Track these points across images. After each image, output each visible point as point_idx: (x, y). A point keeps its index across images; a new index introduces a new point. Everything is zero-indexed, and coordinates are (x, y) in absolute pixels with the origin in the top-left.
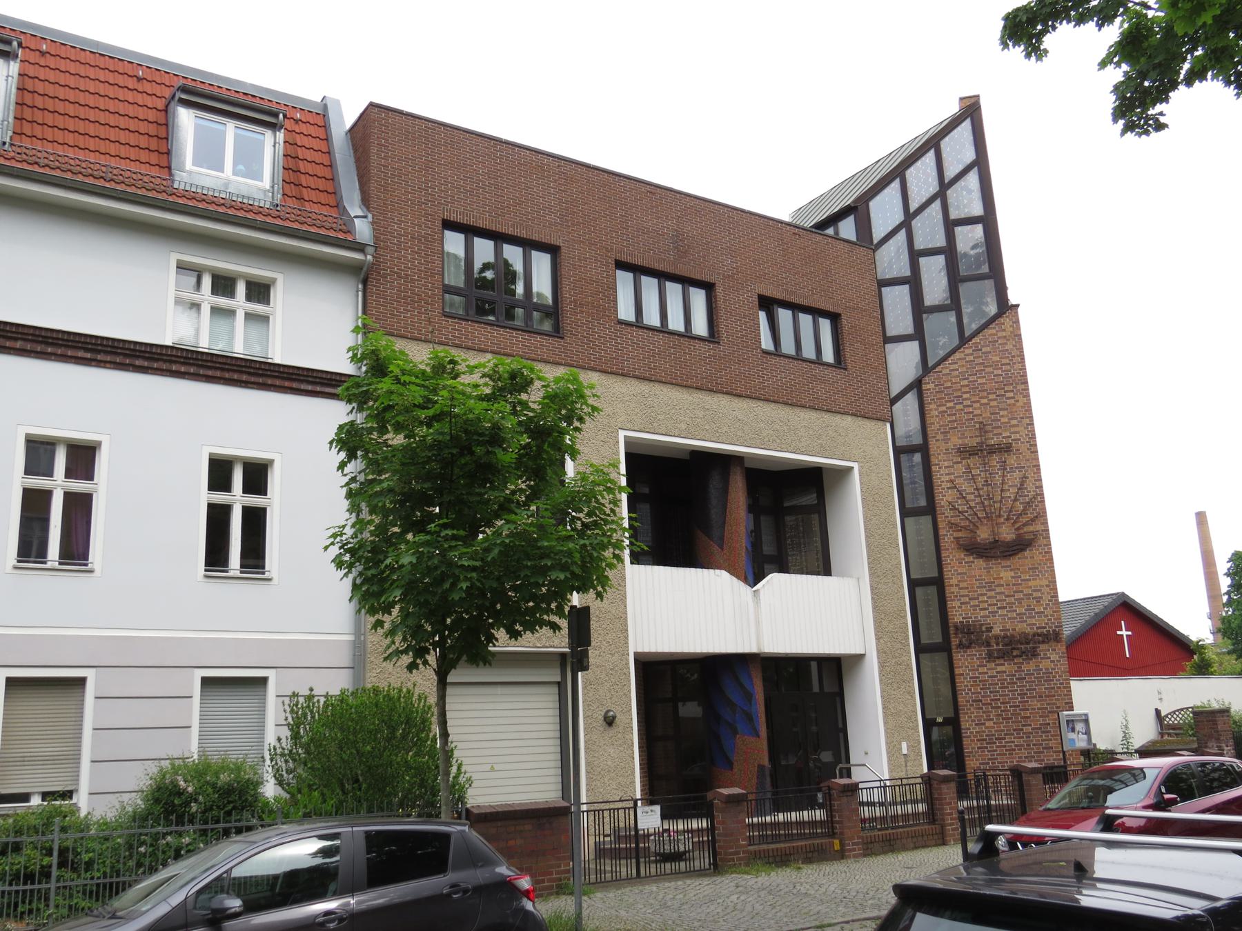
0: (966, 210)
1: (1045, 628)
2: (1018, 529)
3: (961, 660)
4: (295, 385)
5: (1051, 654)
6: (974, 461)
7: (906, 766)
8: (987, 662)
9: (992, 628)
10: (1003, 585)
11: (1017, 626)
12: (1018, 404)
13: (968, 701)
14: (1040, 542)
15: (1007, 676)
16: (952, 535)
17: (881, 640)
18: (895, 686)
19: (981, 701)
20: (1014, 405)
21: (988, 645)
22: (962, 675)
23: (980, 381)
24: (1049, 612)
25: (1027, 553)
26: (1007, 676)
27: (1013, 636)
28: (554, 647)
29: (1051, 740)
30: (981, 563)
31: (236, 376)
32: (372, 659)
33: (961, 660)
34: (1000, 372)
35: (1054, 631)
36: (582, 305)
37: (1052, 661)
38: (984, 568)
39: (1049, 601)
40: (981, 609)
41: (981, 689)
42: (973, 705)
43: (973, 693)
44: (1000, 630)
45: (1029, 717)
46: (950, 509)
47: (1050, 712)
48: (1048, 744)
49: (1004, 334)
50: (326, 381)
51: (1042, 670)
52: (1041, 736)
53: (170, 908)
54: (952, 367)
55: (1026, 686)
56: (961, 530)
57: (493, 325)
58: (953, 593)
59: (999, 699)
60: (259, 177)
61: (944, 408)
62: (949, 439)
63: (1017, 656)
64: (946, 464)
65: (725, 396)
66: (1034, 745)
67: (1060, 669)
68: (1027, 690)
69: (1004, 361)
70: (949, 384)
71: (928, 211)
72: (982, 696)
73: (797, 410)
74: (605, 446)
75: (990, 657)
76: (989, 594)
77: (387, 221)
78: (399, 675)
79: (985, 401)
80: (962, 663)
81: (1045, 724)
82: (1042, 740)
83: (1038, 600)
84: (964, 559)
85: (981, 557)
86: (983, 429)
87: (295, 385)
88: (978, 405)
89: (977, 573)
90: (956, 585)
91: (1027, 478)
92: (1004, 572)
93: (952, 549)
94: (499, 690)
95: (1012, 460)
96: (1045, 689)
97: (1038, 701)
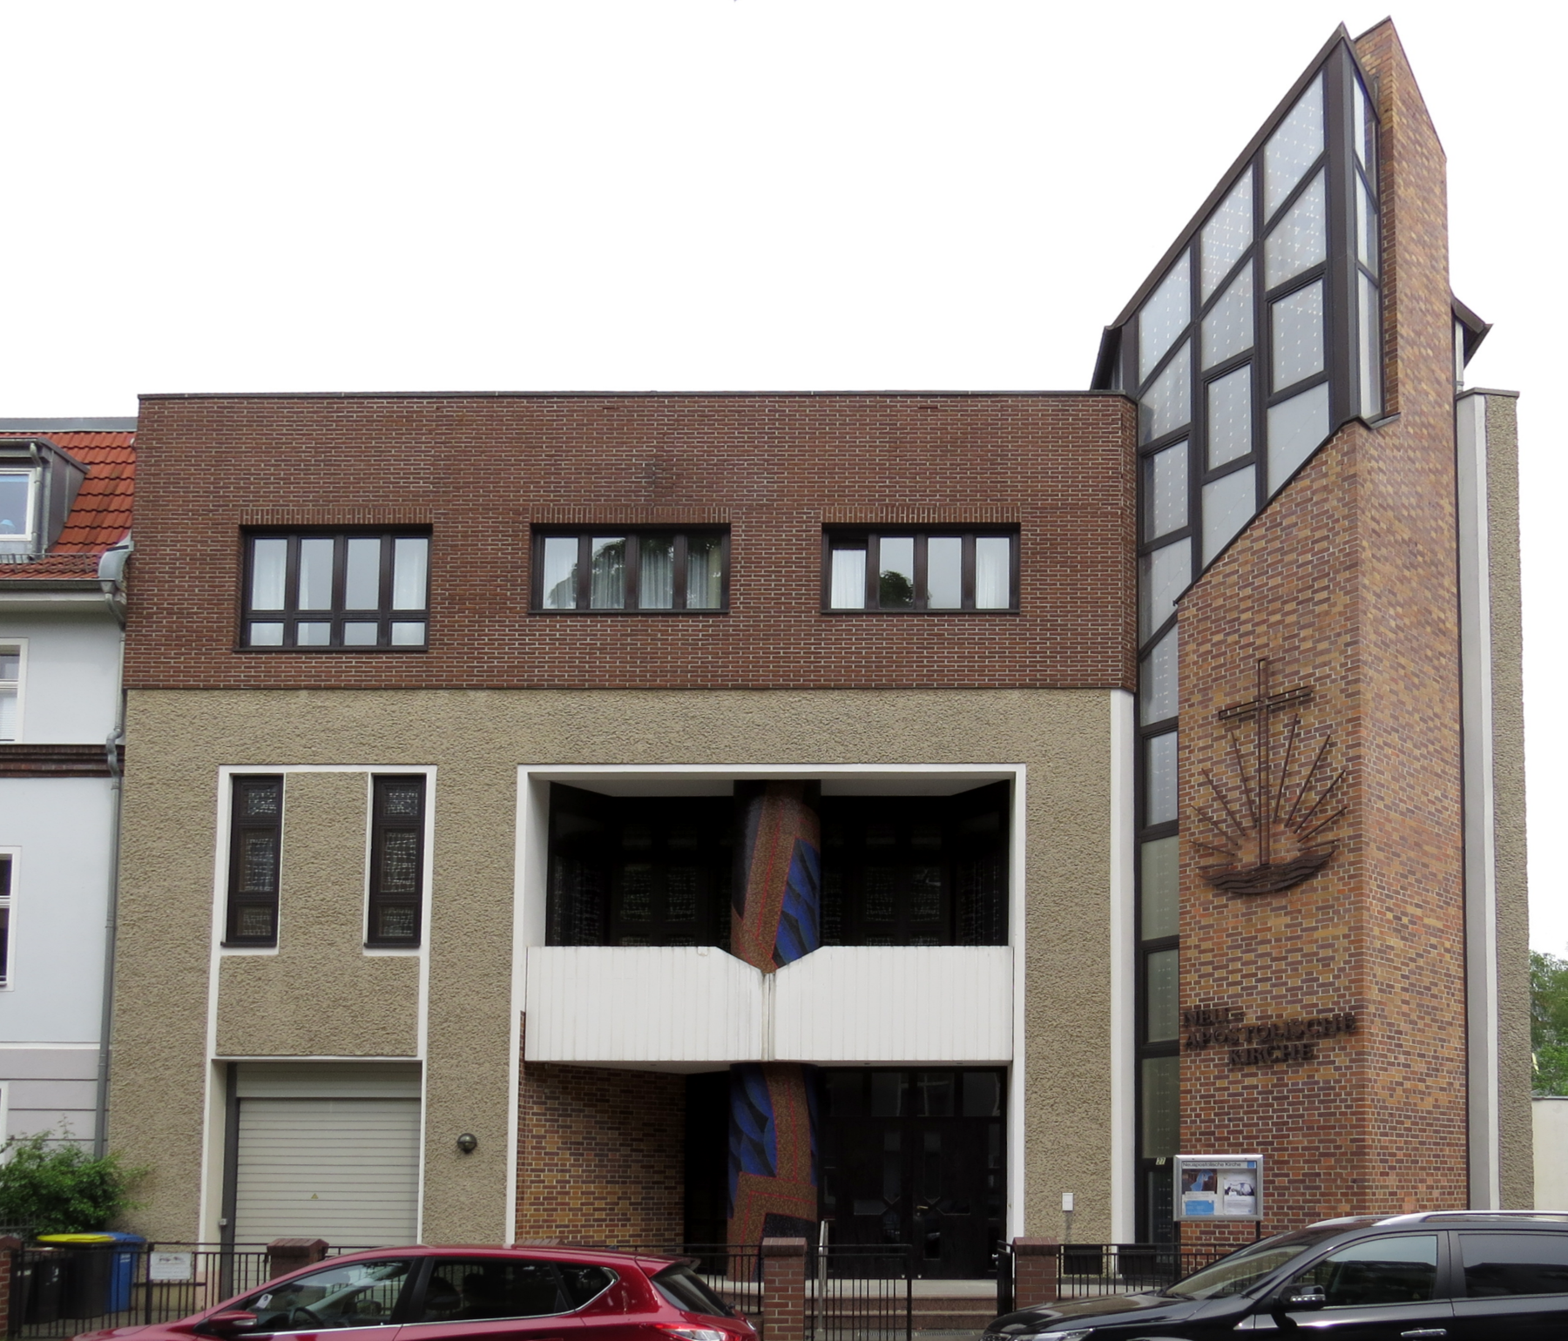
0: (1297, 263)
1: (1333, 1010)
2: (1307, 838)
3: (1190, 1068)
4: (33, 767)
5: (1336, 1056)
6: (1247, 733)
7: (1069, 1228)
8: (1229, 1071)
9: (1243, 1014)
10: (1269, 942)
11: (1286, 1009)
12: (1335, 610)
13: (1194, 1134)
14: (1342, 860)
15: (1259, 1093)
16: (1198, 863)
17: (1039, 1040)
18: (1061, 1108)
19: (1213, 1133)
20: (1327, 613)
21: (1236, 1043)
22: (1190, 1091)
23: (1271, 583)
24: (1343, 981)
25: (1317, 882)
26: (1259, 1093)
27: (1276, 1027)
28: (382, 1055)
29: (1319, 1201)
30: (1239, 905)
31: (23, 766)
32: (117, 1070)
33: (1190, 1068)
34: (1309, 557)
35: (1347, 1015)
36: (462, 600)
37: (1338, 1068)
38: (1243, 915)
39: (1345, 962)
40: (1229, 985)
41: (1216, 1115)
42: (1200, 1140)
43: (1201, 1122)
44: (1257, 1018)
45: (1288, 1162)
46: (1200, 821)
47: (1322, 1155)
48: (1314, 1208)
49: (1324, 482)
50: (74, 757)
51: (1317, 1083)
52: (1304, 1194)
53: (1451, 1315)
54: (1228, 569)
55: (1288, 1110)
56: (1212, 854)
57: (331, 652)
58: (1190, 959)
59: (1241, 1132)
60: (21, 530)
61: (1208, 647)
62: (1211, 699)
63: (1277, 1060)
64: (1201, 744)
65: (733, 693)
66: (1289, 1208)
67: (1350, 1081)
68: (1289, 1117)
69: (1318, 535)
70: (1220, 601)
71: (1232, 290)
72: (1216, 1127)
73: (890, 696)
74: (493, 790)
75: (1236, 1062)
76: (1247, 957)
77: (156, 546)
78: (152, 1088)
79: (1278, 617)
80: (1192, 1074)
81: (1312, 1174)
82: (1304, 1201)
83: (1326, 962)
84: (1212, 902)
85: (1240, 895)
86: (1266, 668)
87: (33, 767)
88: (1264, 628)
89: (1231, 922)
90: (1197, 947)
91: (1333, 745)
92: (1274, 918)
93: (1195, 887)
94: (331, 1107)
95: (1310, 718)
96: (1320, 1115)
97: (1304, 1136)
